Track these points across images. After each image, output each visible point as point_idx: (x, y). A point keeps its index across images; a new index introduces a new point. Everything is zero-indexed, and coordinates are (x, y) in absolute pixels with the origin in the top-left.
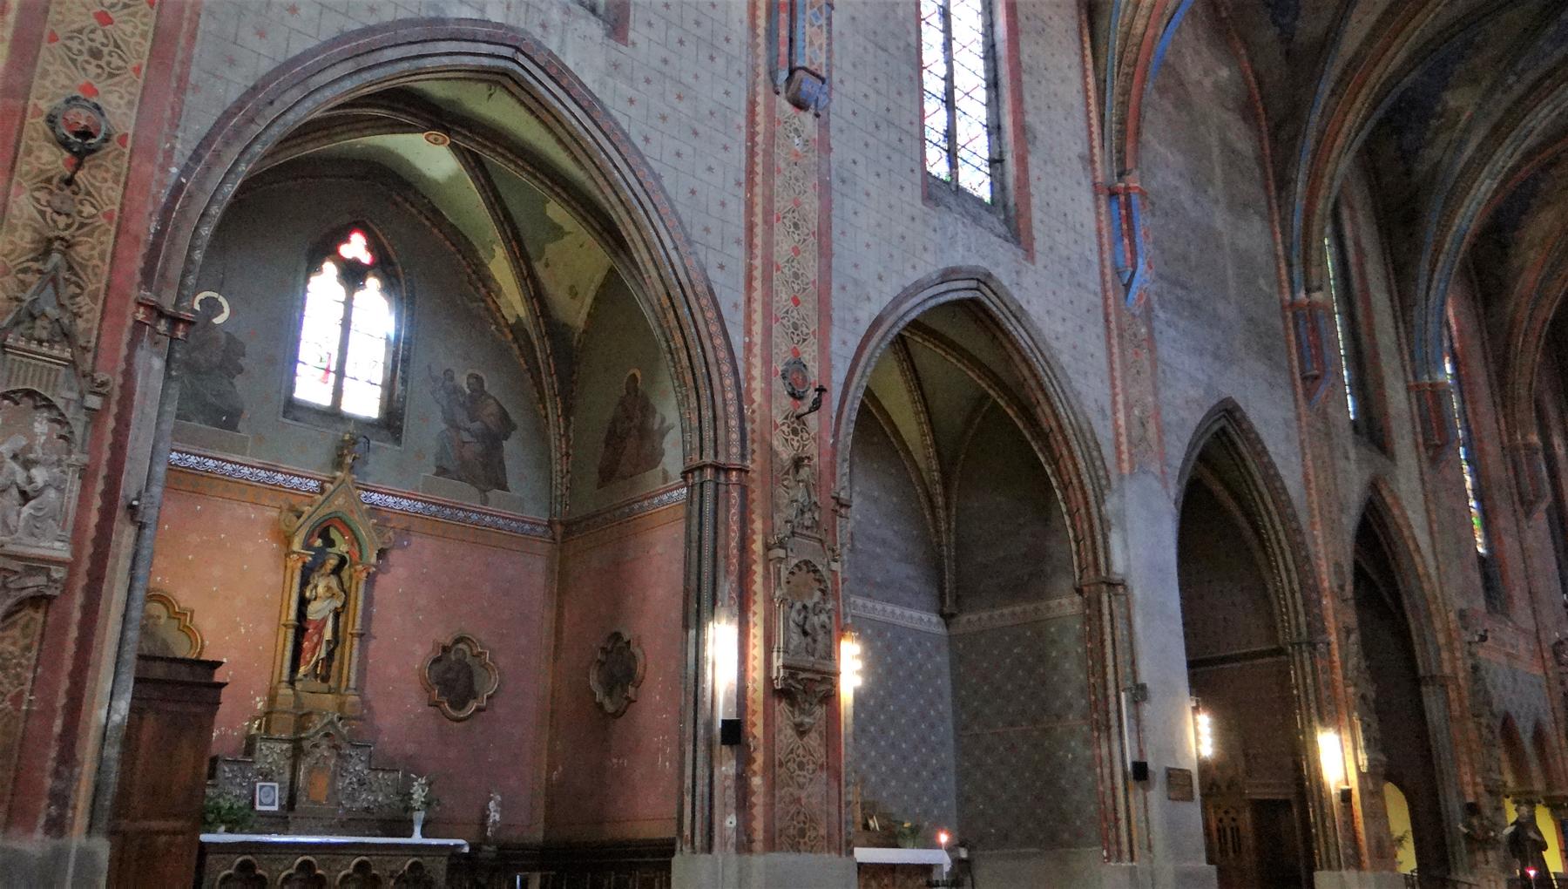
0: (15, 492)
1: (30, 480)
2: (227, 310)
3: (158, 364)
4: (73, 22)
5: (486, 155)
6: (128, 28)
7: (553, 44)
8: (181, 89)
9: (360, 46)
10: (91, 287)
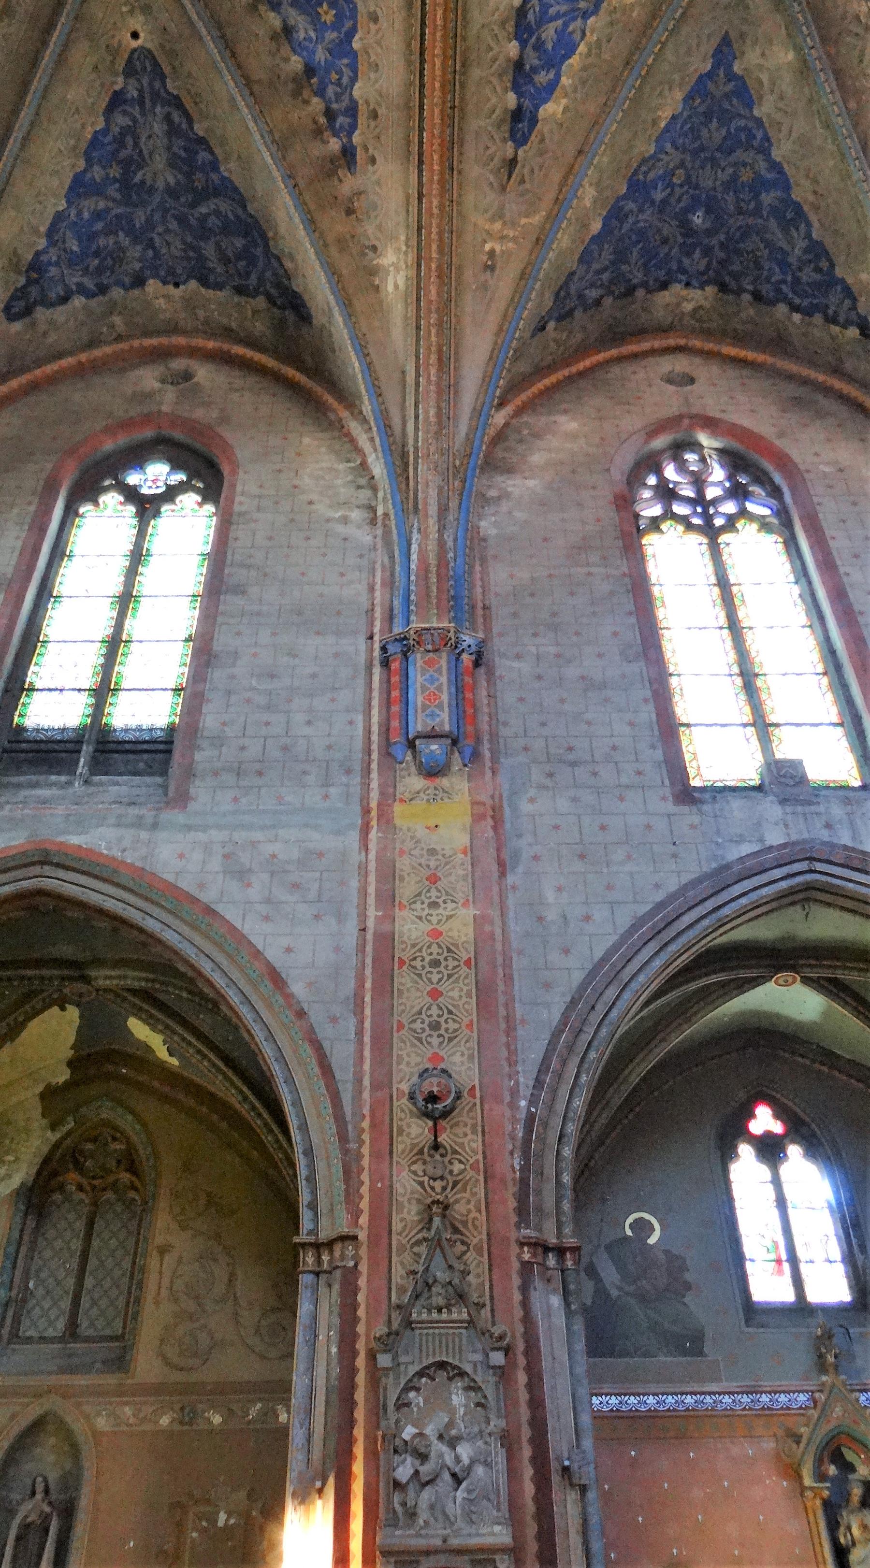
0: (447, 1476)
1: (458, 1460)
2: (657, 1226)
3: (556, 1301)
4: (412, 1007)
5: (840, 975)
6: (455, 994)
7: (845, 838)
8: (510, 1030)
9: (659, 923)
10: (475, 1241)
